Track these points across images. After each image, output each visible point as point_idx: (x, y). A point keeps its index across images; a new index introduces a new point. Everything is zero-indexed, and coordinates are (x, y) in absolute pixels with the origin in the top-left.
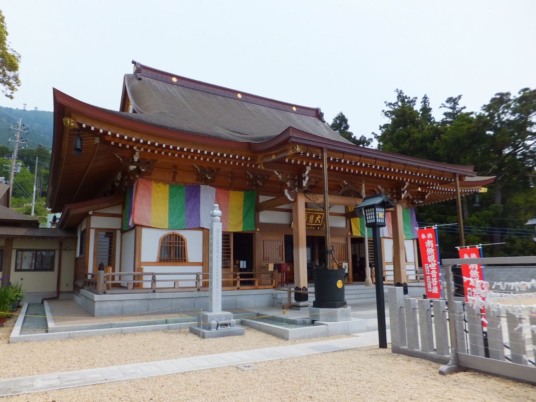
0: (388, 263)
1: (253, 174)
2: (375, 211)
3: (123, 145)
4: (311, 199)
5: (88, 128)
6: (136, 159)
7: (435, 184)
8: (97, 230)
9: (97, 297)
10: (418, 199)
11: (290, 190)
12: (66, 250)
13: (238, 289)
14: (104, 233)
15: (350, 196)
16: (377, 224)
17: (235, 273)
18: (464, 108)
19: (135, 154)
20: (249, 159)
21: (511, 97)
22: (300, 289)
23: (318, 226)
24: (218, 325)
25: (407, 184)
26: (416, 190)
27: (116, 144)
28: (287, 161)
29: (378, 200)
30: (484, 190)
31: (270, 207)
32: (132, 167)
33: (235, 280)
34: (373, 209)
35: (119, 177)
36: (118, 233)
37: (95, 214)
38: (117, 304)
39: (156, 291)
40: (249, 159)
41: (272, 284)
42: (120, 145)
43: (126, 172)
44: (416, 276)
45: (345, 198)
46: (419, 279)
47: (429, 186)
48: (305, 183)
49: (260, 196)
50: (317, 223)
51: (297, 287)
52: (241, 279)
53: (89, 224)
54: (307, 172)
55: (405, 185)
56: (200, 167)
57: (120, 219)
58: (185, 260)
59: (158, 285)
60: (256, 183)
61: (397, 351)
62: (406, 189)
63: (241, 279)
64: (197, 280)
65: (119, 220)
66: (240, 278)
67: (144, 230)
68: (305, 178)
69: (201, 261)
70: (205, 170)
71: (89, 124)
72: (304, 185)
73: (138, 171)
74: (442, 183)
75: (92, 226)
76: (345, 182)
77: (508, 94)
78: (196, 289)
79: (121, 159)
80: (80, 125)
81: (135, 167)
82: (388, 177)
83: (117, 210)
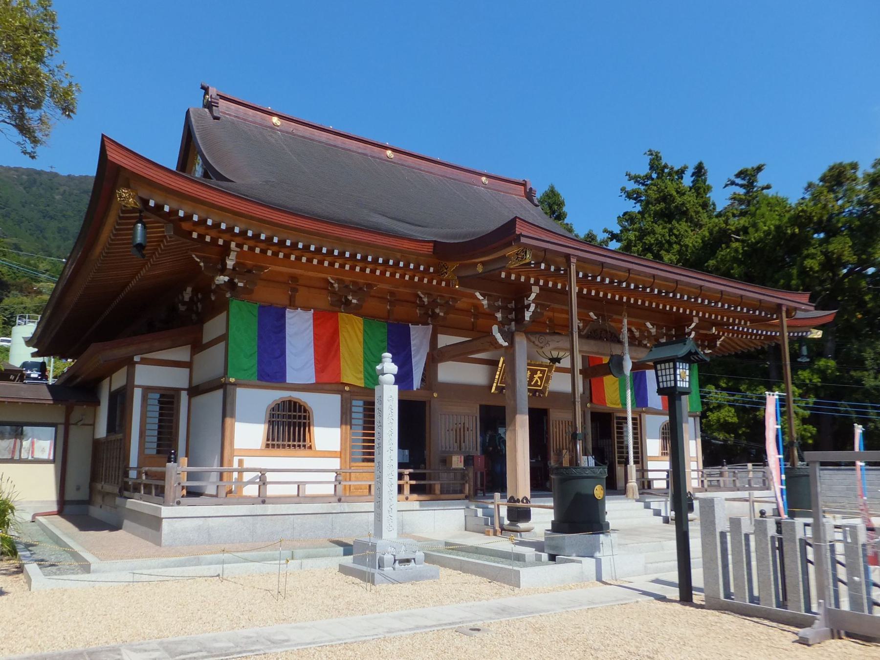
0: (654, 459)
1: (429, 295)
2: (675, 369)
3: (199, 235)
4: (537, 343)
5: (159, 207)
6: (230, 263)
7: (743, 322)
8: (147, 390)
9: (165, 511)
10: (704, 347)
11: (501, 325)
12: (76, 424)
13: (407, 499)
14: (157, 396)
15: (600, 338)
16: (678, 390)
17: (402, 470)
18: (768, 187)
19: (229, 255)
20: (432, 270)
21: (860, 174)
22: (518, 501)
23: (536, 391)
24: (395, 561)
25: (696, 320)
26: (709, 332)
27: (201, 237)
28: (503, 275)
29: (682, 351)
30: (817, 334)
31: (458, 354)
32: (222, 279)
33: (401, 482)
34: (671, 364)
35: (187, 294)
36: (184, 396)
37: (144, 361)
38: (319, 520)
39: (267, 500)
40: (432, 270)
41: (462, 492)
42: (208, 239)
43: (204, 288)
44: (702, 481)
45: (592, 342)
46: (706, 486)
47: (733, 324)
48: (528, 315)
49: (439, 336)
50: (536, 384)
51: (512, 498)
52: (413, 482)
53: (131, 376)
54: (533, 296)
55: (693, 322)
56: (339, 281)
57: (187, 371)
58: (310, 447)
59: (272, 491)
60: (433, 312)
61: (712, 605)
62: (692, 330)
63: (413, 482)
64: (337, 483)
65: (186, 371)
66: (410, 479)
67: (239, 391)
68: (528, 307)
69: (339, 449)
70: (347, 287)
71: (160, 200)
72: (527, 318)
73: (231, 284)
74: (754, 320)
75: (136, 383)
76: (591, 314)
77: (854, 166)
78: (336, 499)
79: (202, 264)
80: (145, 202)
81: (226, 279)
82: (661, 307)
83: (182, 354)
